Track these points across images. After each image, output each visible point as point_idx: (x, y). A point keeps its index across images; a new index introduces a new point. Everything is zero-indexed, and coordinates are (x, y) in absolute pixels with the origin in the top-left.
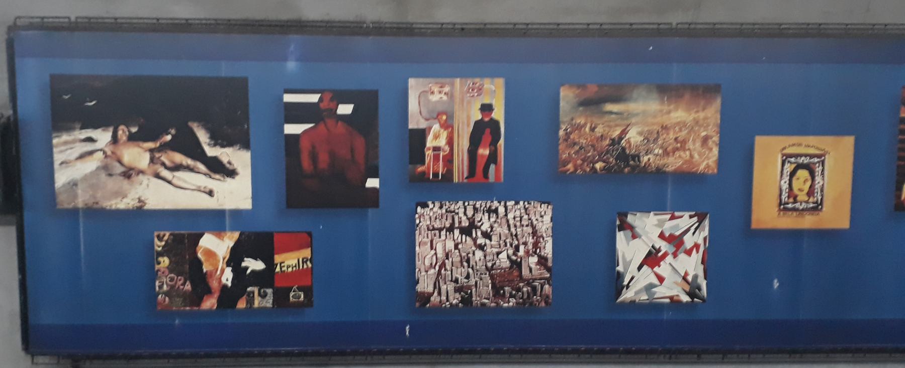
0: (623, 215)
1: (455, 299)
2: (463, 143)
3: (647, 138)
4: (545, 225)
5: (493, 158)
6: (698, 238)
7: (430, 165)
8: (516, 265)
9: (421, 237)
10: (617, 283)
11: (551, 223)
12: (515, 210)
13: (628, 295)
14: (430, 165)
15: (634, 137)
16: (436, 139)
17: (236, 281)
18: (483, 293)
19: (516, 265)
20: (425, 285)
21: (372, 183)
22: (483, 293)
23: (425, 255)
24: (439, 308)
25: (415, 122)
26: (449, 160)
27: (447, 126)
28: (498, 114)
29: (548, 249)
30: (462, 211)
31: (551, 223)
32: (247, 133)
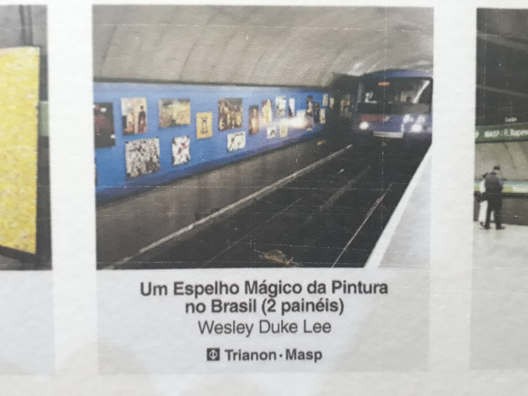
0: (173, 139)
1: (137, 173)
2: (137, 119)
3: (166, 118)
4: (157, 145)
5: (144, 124)
6: (188, 144)
7: (129, 129)
8: (151, 159)
9: (127, 154)
10: (173, 159)
11: (189, 139)
12: (150, 142)
13: (176, 162)
14: (129, 129)
15: (175, 115)
16: (130, 119)
17: (384, 144)
18: (144, 169)
19: (151, 159)
20: (129, 171)
21: (113, 136)
22: (144, 169)
23: (129, 160)
24: (133, 178)
25: (124, 113)
26: (133, 126)
27: (132, 114)
28: (145, 110)
29: (158, 153)
30: (138, 143)
31: (189, 139)
32: (480, 27)
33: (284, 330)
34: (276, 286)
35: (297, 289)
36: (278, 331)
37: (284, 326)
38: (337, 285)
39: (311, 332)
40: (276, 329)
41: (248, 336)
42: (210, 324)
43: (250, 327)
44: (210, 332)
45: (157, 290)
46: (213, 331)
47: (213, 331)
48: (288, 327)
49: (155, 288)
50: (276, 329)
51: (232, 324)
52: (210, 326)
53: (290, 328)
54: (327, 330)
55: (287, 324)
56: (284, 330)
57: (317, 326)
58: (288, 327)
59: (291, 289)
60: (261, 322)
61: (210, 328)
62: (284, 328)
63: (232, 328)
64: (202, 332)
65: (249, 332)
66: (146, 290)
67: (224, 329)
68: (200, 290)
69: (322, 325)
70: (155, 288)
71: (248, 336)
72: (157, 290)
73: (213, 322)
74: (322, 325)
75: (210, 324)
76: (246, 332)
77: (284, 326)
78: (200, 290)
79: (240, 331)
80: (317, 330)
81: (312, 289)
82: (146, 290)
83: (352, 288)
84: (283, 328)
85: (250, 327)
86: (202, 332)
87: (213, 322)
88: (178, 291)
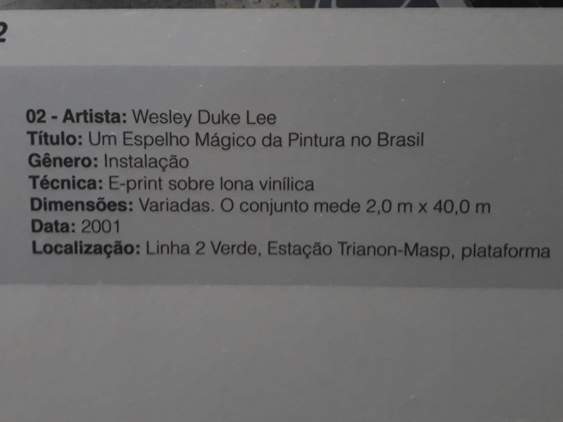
33: (225, 121)
34: (229, 138)
35: (251, 141)
36: (219, 122)
37: (225, 116)
38: (293, 137)
39: (255, 123)
40: (216, 120)
41: (186, 126)
42: (144, 113)
43: (188, 117)
44: (145, 121)
45: (106, 139)
46: (148, 120)
47: (148, 120)
48: (229, 118)
49: (104, 137)
50: (216, 120)
51: (168, 114)
52: (144, 114)
53: (232, 119)
54: (272, 121)
55: (228, 115)
56: (225, 121)
57: (261, 117)
58: (229, 118)
59: (245, 141)
60: (200, 111)
61: (144, 118)
62: (225, 118)
63: (168, 118)
64: (137, 121)
65: (188, 122)
66: (95, 141)
67: (159, 119)
68: (149, 141)
69: (266, 117)
70: (111, 159)
71: (186, 126)
72: (106, 139)
73: (147, 111)
74: (266, 117)
75: (144, 113)
76: (184, 122)
77: (225, 116)
78: (149, 141)
79: (178, 121)
80: (261, 121)
81: (267, 142)
82: (95, 141)
83: (308, 141)
84: (223, 119)
85: (188, 117)
86: (137, 121)
87: (147, 111)
88: (128, 142)
